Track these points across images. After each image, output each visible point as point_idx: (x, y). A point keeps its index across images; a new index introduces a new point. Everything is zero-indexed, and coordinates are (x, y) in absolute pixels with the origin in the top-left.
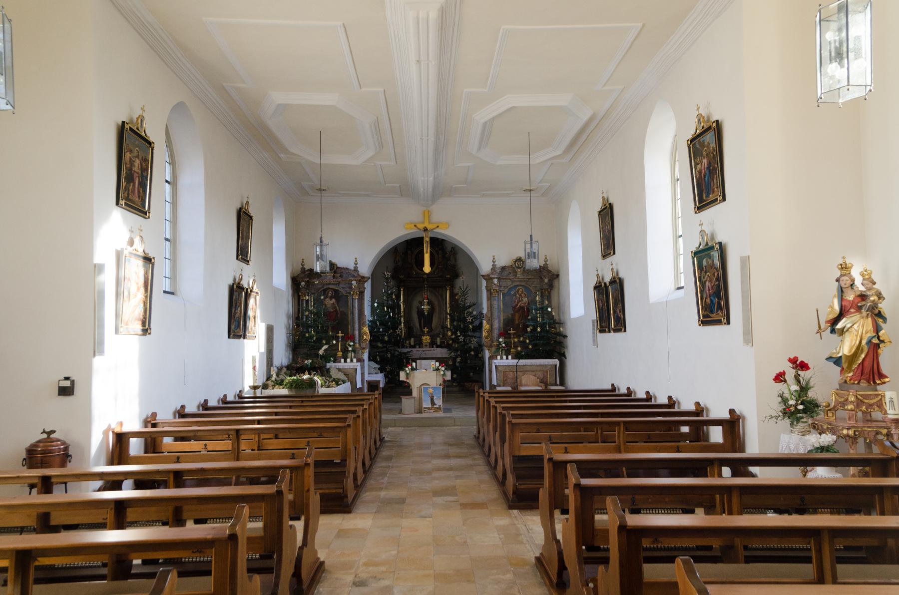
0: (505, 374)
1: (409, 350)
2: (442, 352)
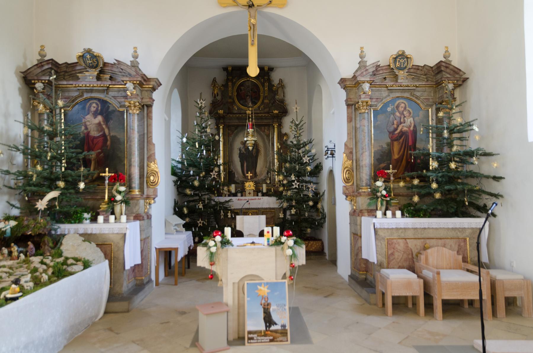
0: (390, 243)
1: (228, 198)
2: (270, 202)
